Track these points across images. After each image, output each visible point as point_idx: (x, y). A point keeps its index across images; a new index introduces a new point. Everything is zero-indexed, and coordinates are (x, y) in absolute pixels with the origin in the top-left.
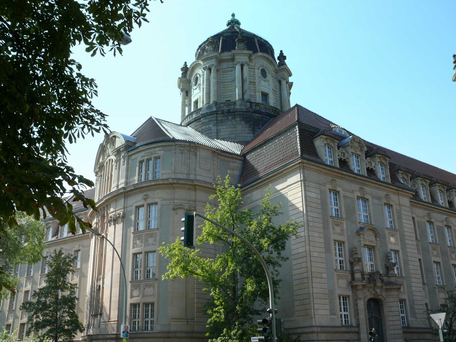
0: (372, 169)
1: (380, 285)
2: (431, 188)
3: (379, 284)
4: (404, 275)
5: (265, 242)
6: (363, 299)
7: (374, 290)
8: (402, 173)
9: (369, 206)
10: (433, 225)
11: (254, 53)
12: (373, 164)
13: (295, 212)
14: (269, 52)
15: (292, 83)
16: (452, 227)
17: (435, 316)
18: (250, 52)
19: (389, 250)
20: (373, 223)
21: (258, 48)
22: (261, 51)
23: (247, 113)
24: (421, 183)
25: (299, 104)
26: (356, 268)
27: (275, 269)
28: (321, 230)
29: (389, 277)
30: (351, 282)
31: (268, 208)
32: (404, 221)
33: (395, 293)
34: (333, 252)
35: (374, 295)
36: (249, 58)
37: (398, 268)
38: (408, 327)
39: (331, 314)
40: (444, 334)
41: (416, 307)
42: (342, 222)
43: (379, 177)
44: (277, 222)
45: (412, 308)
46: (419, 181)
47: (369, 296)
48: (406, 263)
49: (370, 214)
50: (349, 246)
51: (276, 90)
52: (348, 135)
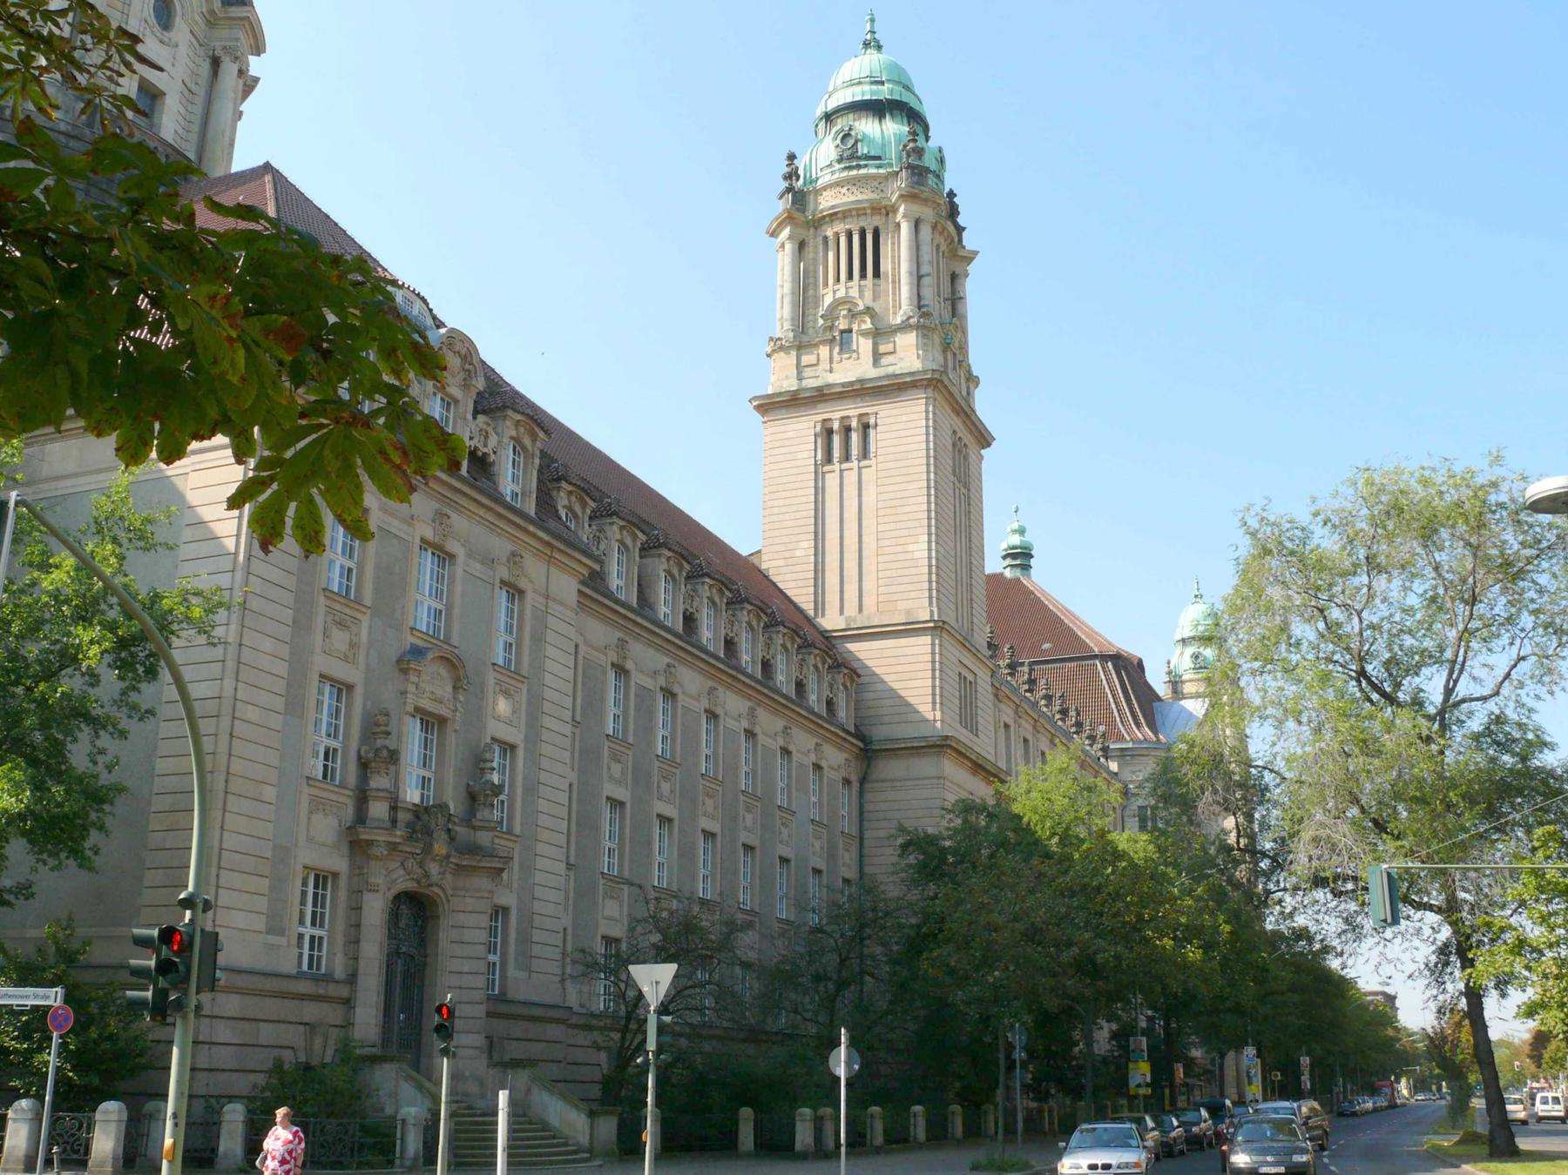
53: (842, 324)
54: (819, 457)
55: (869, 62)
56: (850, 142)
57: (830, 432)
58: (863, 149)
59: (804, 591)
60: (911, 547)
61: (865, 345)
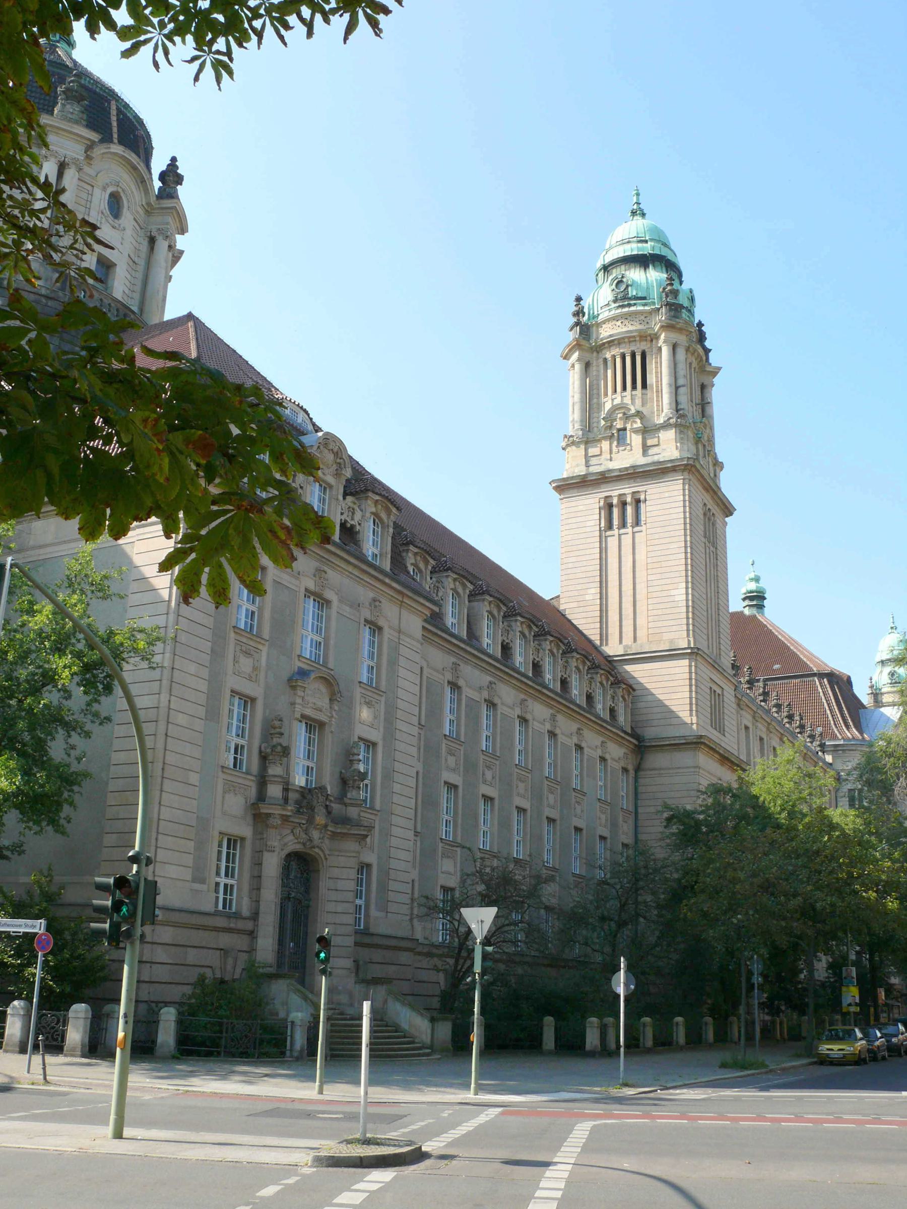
0: (353, 526)
1: (323, 822)
2: (475, 604)
3: (320, 818)
4: (378, 807)
5: (64, 666)
6: (277, 849)
7: (306, 832)
8: (416, 554)
9: (328, 619)
10: (460, 694)
11: (102, 141)
12: (358, 515)
13: (147, 598)
14: (142, 151)
15: (182, 252)
16: (499, 706)
17: (469, 914)
18: (94, 136)
19: (356, 740)
20: (331, 665)
21: (115, 130)
22: (121, 142)
23: (50, 303)
24: (452, 586)
25: (196, 313)
26: (275, 770)
27: (70, 740)
28: (206, 659)
29: (346, 805)
30: (254, 805)
31: (86, 576)
32: (402, 672)
33: (351, 845)
34: (225, 720)
35: (304, 844)
36: (85, 152)
37: (367, 785)
38: (366, 933)
39: (195, 880)
40: (485, 956)
41: (392, 885)
42: (260, 647)
43: (364, 551)
44: (101, 617)
45: (383, 888)
46: (449, 582)
47: (293, 846)
48: (388, 776)
49: (327, 639)
50: (264, 712)
51: (136, 260)
52: (310, 427)
53: (619, 424)
54: (603, 525)
55: (636, 226)
56: (623, 287)
57: (610, 506)
58: (632, 292)
59: (592, 626)
60: (673, 593)
61: (636, 440)
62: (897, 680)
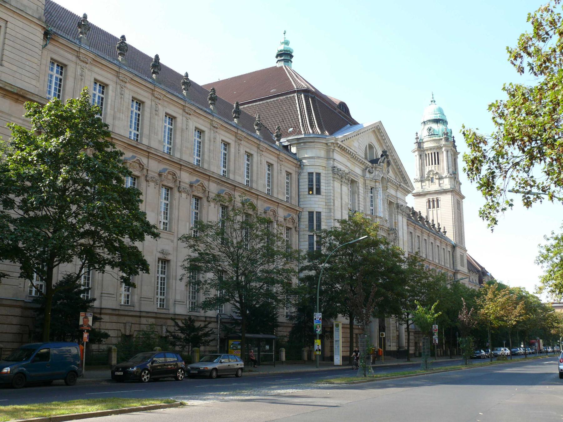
53: (431, 176)
55: (434, 107)
57: (429, 201)
62: (433, 133)
